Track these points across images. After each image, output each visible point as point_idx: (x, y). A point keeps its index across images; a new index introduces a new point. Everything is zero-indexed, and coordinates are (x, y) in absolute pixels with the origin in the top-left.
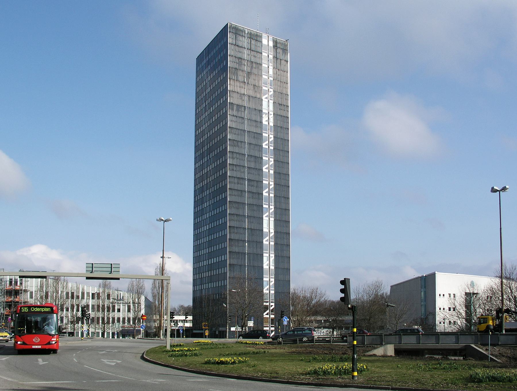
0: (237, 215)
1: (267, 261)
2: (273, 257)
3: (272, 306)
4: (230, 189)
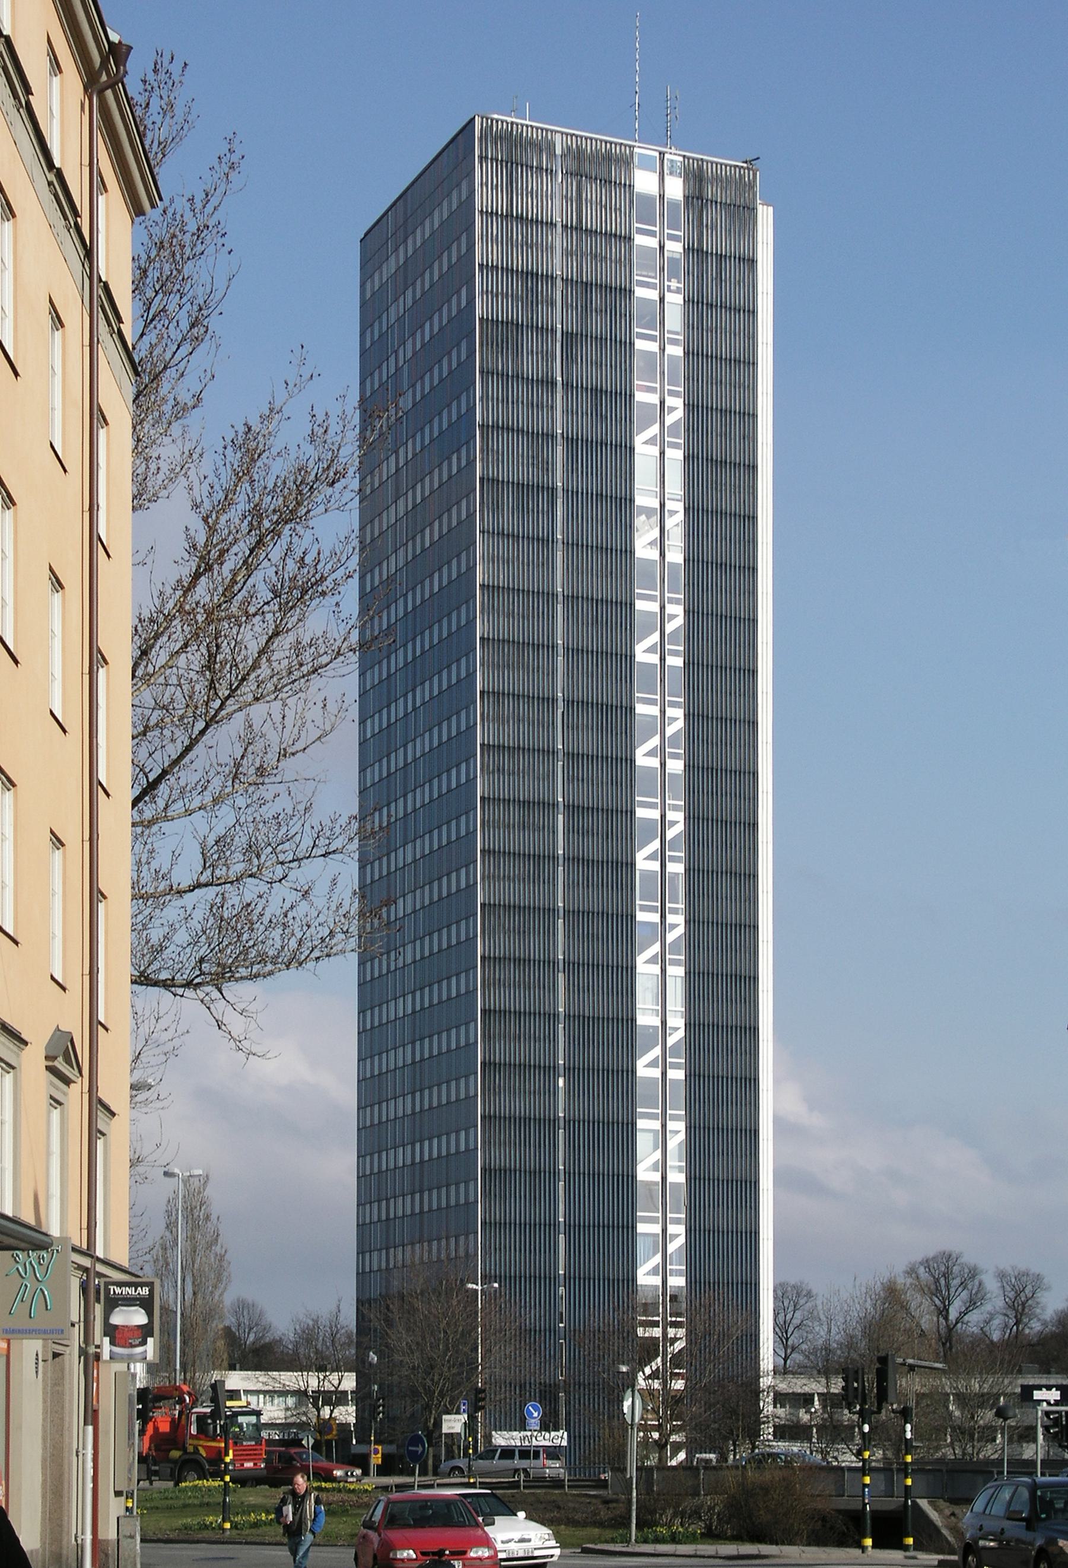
0: (517, 961)
1: (655, 1148)
2: (677, 512)
3: (674, 1340)
4: (489, 851)
